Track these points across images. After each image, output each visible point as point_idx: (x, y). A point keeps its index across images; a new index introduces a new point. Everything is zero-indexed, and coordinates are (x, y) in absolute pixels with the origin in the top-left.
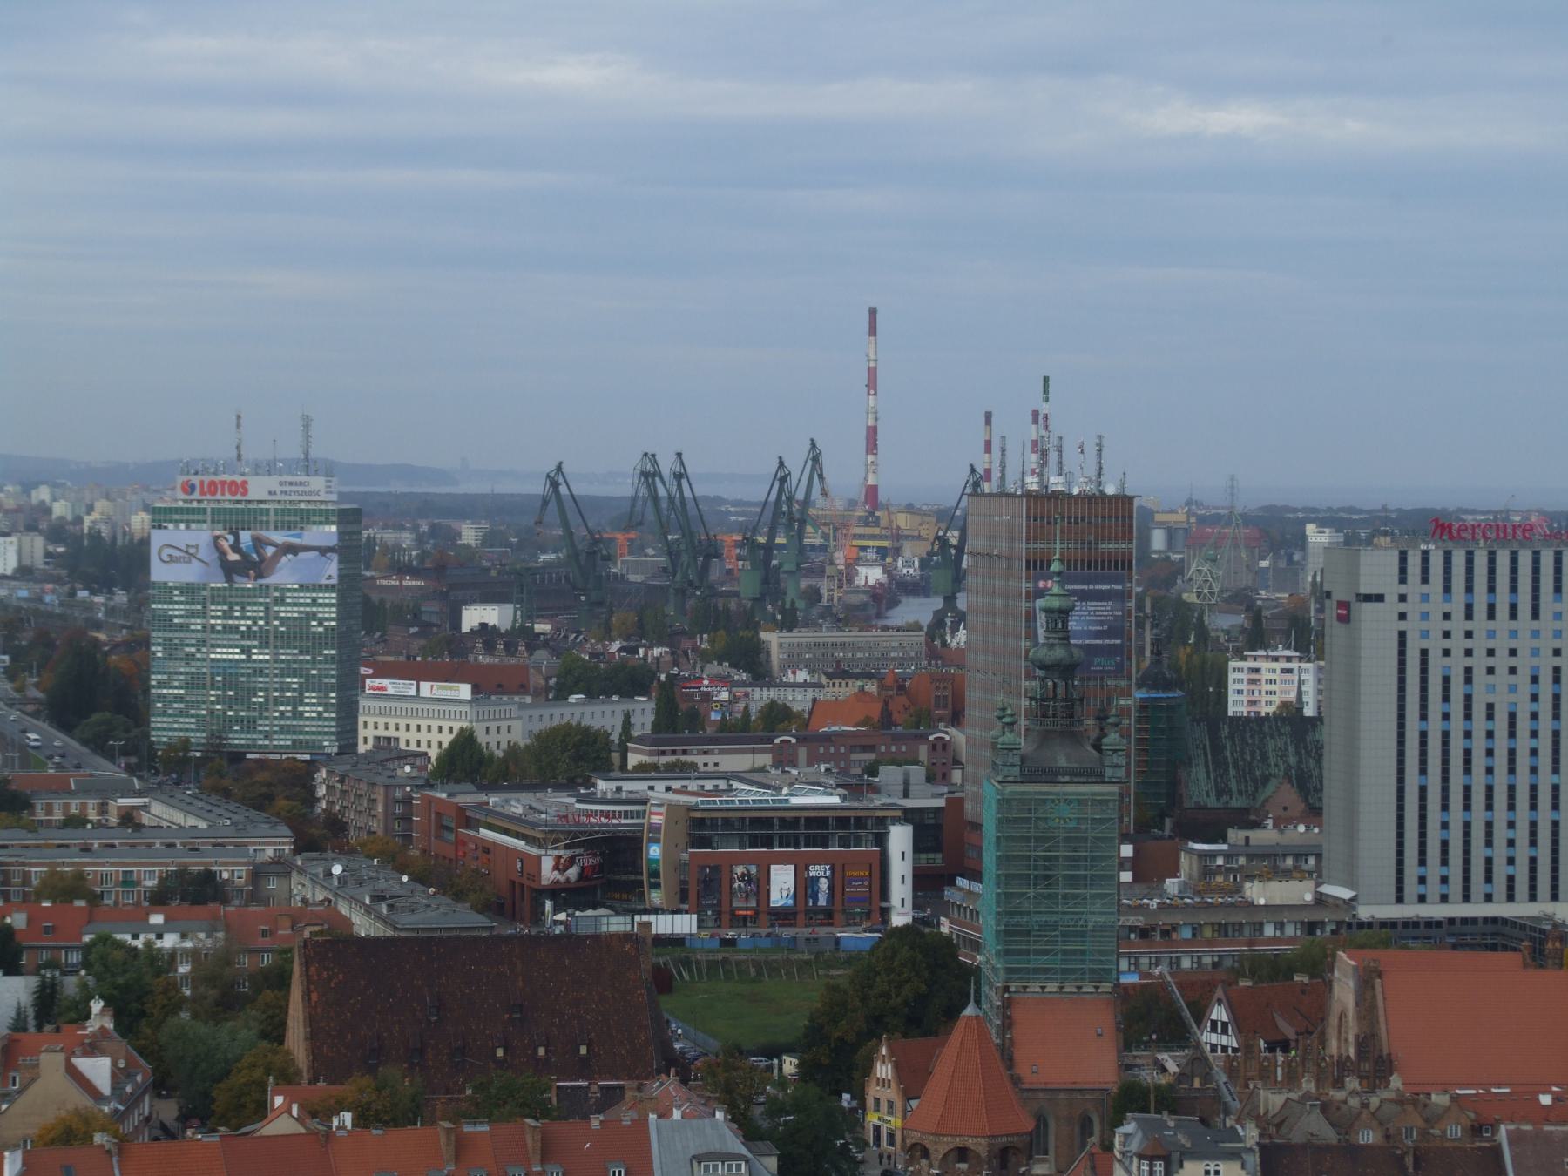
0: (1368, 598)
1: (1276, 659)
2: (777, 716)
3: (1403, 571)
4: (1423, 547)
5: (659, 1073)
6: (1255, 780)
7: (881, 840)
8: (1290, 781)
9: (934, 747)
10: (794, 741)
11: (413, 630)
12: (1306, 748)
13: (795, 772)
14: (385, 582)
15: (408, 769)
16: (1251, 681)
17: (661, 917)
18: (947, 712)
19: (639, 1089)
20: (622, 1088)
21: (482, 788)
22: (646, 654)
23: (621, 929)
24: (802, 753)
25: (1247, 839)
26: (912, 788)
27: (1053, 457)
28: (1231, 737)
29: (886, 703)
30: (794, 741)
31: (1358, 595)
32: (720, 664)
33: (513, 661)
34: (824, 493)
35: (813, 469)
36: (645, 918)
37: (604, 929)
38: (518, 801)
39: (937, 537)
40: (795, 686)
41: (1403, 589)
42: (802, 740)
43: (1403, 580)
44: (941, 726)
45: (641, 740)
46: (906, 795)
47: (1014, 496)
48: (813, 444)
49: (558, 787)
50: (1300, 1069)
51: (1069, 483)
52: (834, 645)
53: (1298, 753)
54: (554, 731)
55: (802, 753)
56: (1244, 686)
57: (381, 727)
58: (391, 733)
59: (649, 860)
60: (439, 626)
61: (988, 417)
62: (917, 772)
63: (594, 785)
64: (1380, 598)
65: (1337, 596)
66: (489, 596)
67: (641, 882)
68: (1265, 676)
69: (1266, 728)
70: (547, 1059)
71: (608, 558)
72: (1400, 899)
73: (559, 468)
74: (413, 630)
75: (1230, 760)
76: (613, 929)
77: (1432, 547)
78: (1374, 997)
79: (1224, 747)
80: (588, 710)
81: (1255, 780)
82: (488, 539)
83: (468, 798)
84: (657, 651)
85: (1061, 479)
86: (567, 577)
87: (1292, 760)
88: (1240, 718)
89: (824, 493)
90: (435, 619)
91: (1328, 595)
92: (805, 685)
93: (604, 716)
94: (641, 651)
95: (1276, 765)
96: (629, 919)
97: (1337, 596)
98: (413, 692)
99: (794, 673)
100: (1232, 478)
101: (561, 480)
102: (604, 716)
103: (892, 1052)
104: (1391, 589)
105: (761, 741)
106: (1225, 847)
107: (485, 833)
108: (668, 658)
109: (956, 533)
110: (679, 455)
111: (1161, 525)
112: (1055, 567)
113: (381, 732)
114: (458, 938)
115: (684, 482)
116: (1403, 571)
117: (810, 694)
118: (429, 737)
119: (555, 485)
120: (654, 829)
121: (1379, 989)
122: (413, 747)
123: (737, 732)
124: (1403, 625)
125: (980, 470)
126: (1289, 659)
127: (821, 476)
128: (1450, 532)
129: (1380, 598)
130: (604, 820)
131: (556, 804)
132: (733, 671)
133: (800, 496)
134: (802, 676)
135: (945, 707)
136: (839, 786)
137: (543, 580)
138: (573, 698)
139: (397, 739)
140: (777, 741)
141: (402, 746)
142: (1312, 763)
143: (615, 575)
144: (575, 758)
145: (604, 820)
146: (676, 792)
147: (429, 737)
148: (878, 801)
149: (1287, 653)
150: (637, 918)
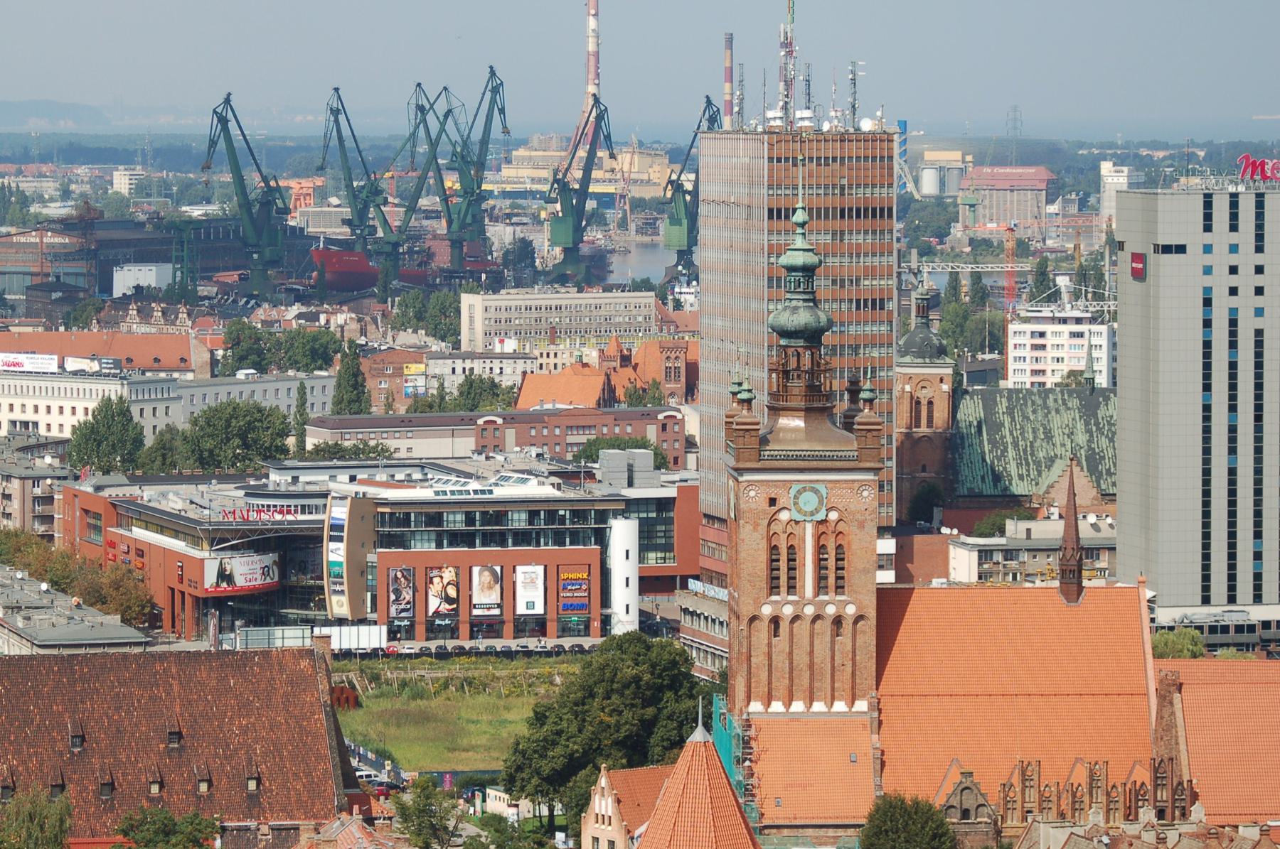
0: (1167, 249)
1: (1064, 321)
2: (479, 393)
3: (1208, 217)
4: (1232, 189)
5: (341, 810)
6: (1038, 463)
7: (601, 538)
8: (1079, 464)
9: (664, 427)
10: (500, 421)
11: (55, 295)
12: (1097, 424)
13: (500, 458)
14: (22, 239)
15: (48, 460)
16: (1036, 347)
17: (345, 629)
18: (681, 386)
19: (317, 831)
20: (296, 828)
21: (134, 480)
22: (328, 321)
23: (299, 643)
24: (510, 435)
25: (1029, 530)
26: (636, 476)
27: (799, 86)
28: (1010, 411)
29: (608, 376)
30: (500, 421)
31: (1156, 246)
32: (415, 331)
33: (171, 329)
34: (506, 130)
35: (493, 101)
36: (326, 631)
37: (278, 643)
38: (177, 494)
39: (670, 182)
40: (503, 356)
41: (1208, 238)
42: (509, 420)
43: (1208, 228)
44: (673, 402)
45: (321, 423)
46: (630, 484)
47: (755, 132)
48: (493, 73)
49: (224, 479)
50: (1086, 799)
51: (818, 120)
52: (549, 308)
53: (1089, 432)
54: (234, 410)
55: (510, 435)
56: (1027, 353)
57: (17, 408)
58: (29, 416)
59: (328, 562)
60: (85, 290)
61: (730, 40)
62: (643, 457)
63: (267, 476)
64: (1181, 249)
65: (1130, 248)
66: (144, 256)
67: (322, 588)
68: (1049, 341)
69: (1050, 402)
70: (210, 796)
71: (286, 211)
72: (1206, 600)
73: (227, 101)
74: (55, 295)
75: (1009, 439)
76: (289, 643)
77: (1241, 188)
78: (1173, 713)
79: (1002, 425)
80: (259, 388)
81: (1038, 463)
82: (141, 188)
83: (120, 490)
84: (340, 318)
85: (807, 114)
86: (236, 231)
87: (1081, 438)
88: (1018, 391)
89: (506, 130)
90: (81, 282)
91: (1121, 245)
92: (514, 356)
93: (273, 392)
94: (323, 318)
95: (1063, 445)
96: (308, 633)
97: (1130, 248)
98: (55, 369)
99: (502, 341)
100: (1015, 109)
101: (230, 116)
102: (273, 392)
103: (612, 787)
104: (1193, 236)
105: (461, 421)
106: (1003, 541)
107: (139, 533)
108: (355, 326)
109: (692, 177)
110: (337, 90)
111: (931, 165)
112: (800, 216)
113: (18, 415)
114: (105, 655)
115: (342, 118)
116: (1208, 217)
117: (520, 365)
118: (61, 419)
119: (223, 121)
120: (337, 527)
121: (1178, 706)
122: (55, 433)
123: (429, 412)
124: (1259, 259)
125: (718, 102)
126: (1079, 321)
127: (502, 111)
128: (1263, 171)
129: (1181, 249)
130: (278, 517)
131: (222, 500)
132: (430, 340)
133: (477, 135)
134: (511, 345)
135: (677, 381)
136: (552, 474)
137: (208, 234)
138: (241, 375)
139: (36, 424)
140: (480, 422)
141: (42, 431)
142: (1104, 442)
143: (293, 228)
144: (238, 442)
145: (278, 517)
146: (362, 482)
147: (61, 419)
148: (599, 491)
149: (1077, 314)
150: (317, 631)
